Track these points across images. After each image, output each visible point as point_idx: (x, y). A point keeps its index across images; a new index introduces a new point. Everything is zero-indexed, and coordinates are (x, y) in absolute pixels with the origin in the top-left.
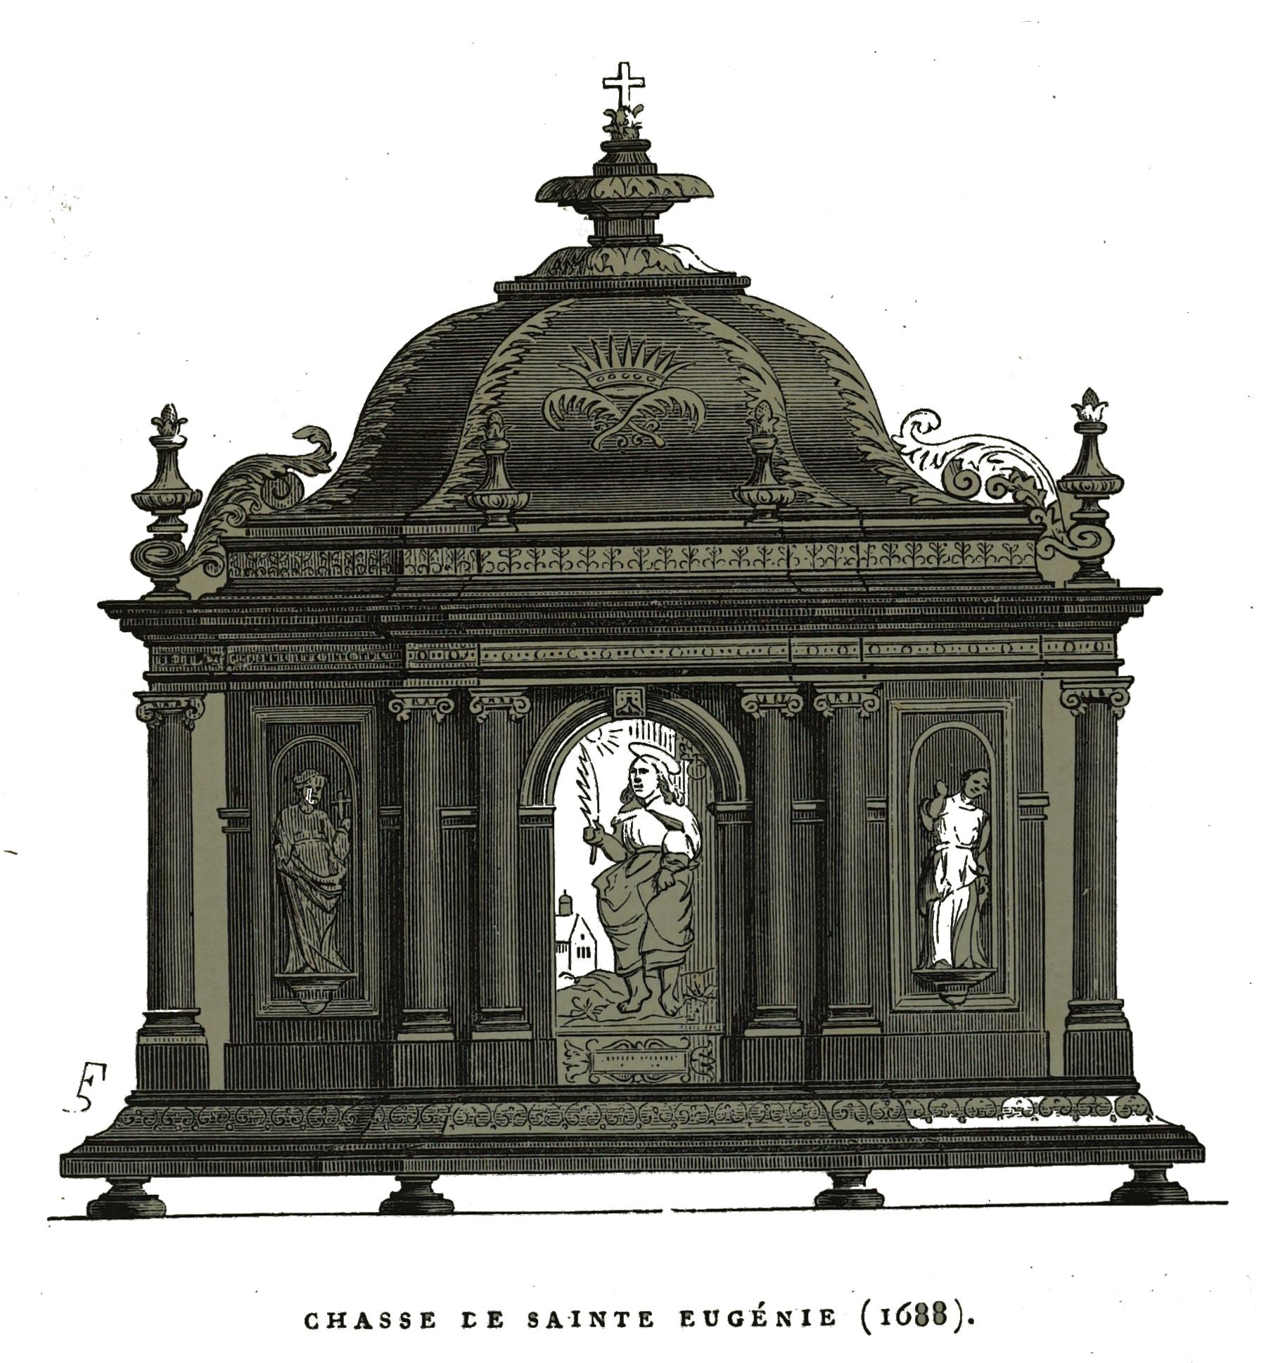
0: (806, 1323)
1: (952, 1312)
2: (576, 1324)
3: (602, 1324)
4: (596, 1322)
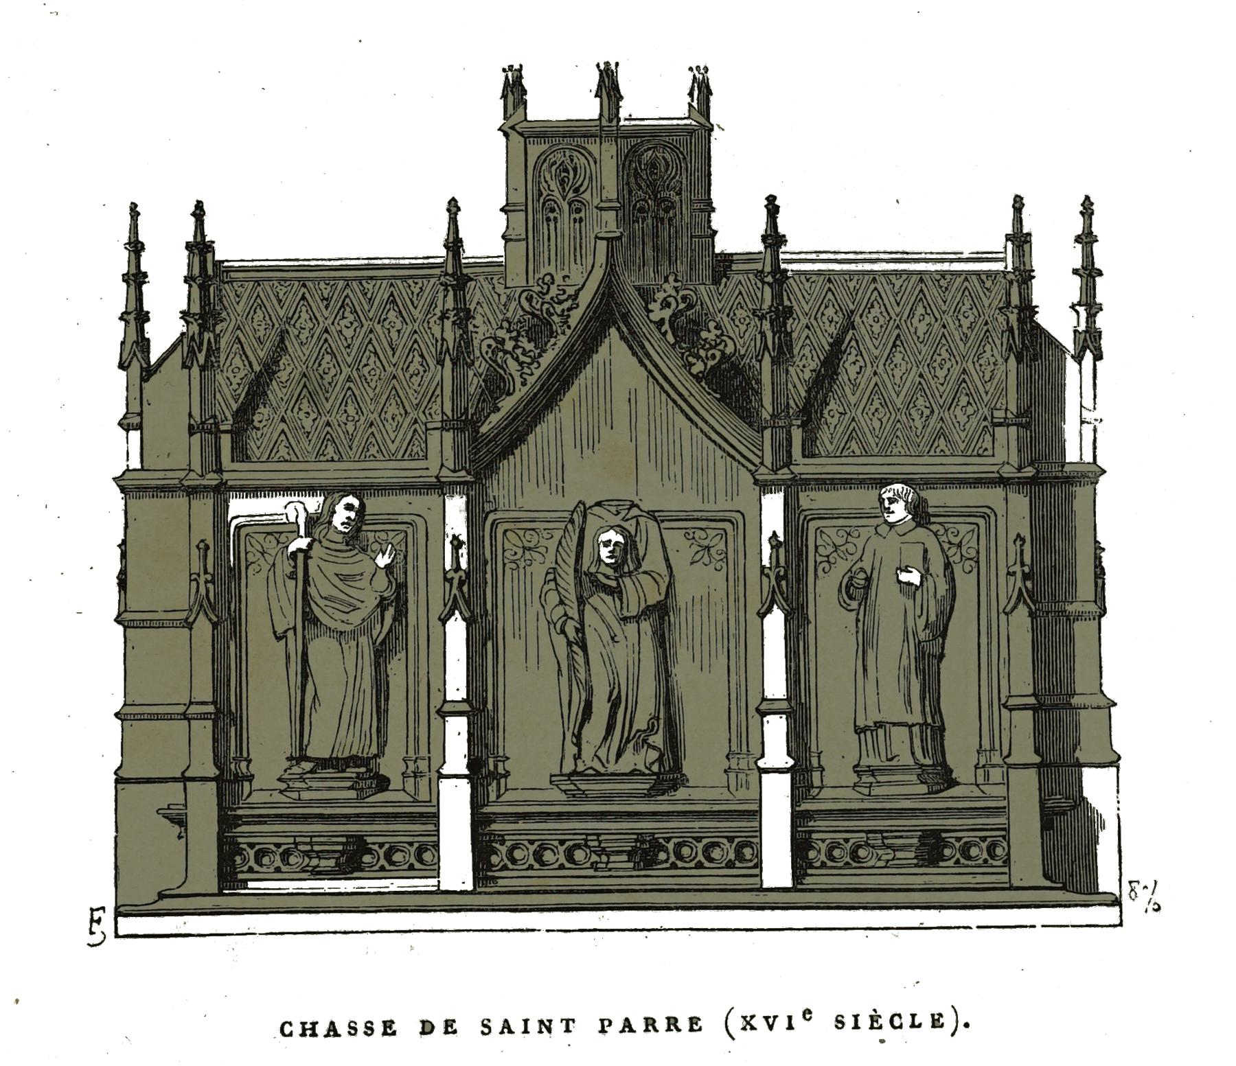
0: (856, 1027)
1: (949, 1020)
2: (526, 1031)
4: (544, 1029)
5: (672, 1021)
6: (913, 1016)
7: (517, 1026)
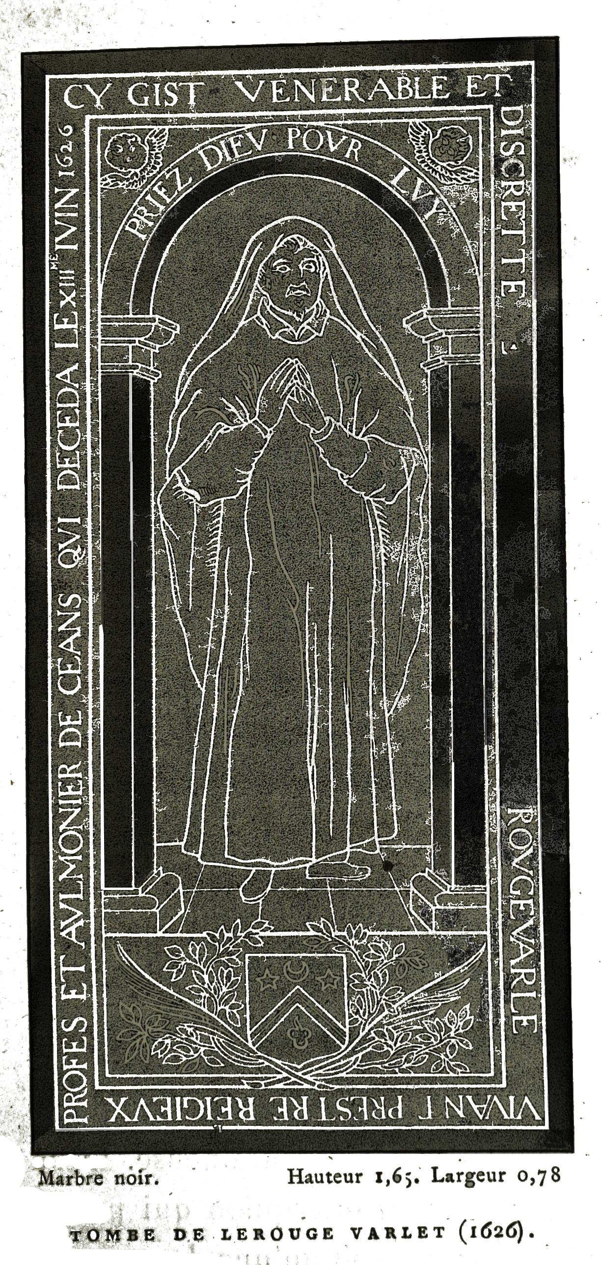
5: (390, 1231)
6: (405, 1229)
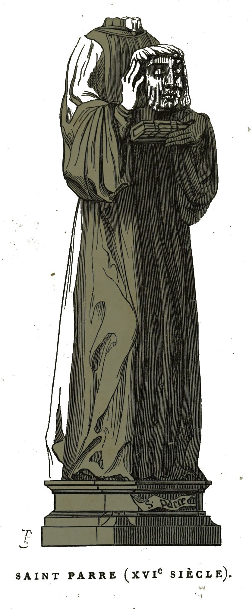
0: (181, 577)
1: (223, 573)
2: (36, 579)
3: (47, 578)
4: (44, 577)
5: (102, 574)
6: (208, 572)
7: (32, 576)
